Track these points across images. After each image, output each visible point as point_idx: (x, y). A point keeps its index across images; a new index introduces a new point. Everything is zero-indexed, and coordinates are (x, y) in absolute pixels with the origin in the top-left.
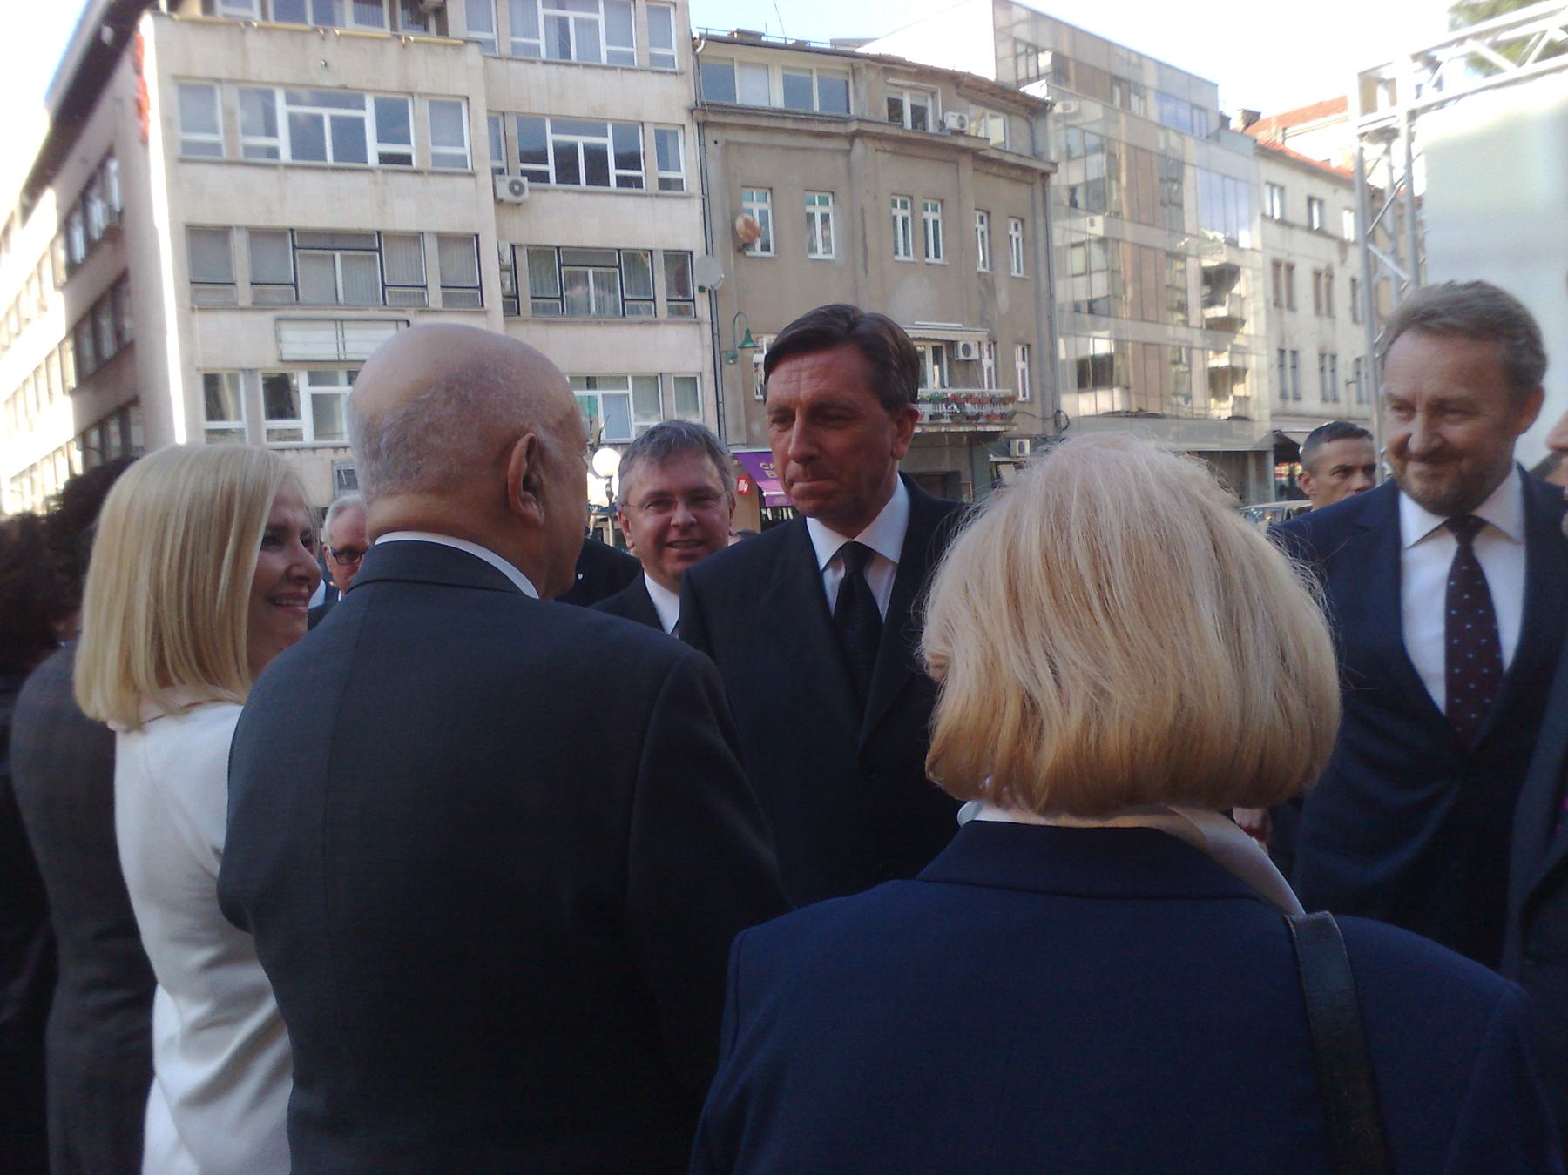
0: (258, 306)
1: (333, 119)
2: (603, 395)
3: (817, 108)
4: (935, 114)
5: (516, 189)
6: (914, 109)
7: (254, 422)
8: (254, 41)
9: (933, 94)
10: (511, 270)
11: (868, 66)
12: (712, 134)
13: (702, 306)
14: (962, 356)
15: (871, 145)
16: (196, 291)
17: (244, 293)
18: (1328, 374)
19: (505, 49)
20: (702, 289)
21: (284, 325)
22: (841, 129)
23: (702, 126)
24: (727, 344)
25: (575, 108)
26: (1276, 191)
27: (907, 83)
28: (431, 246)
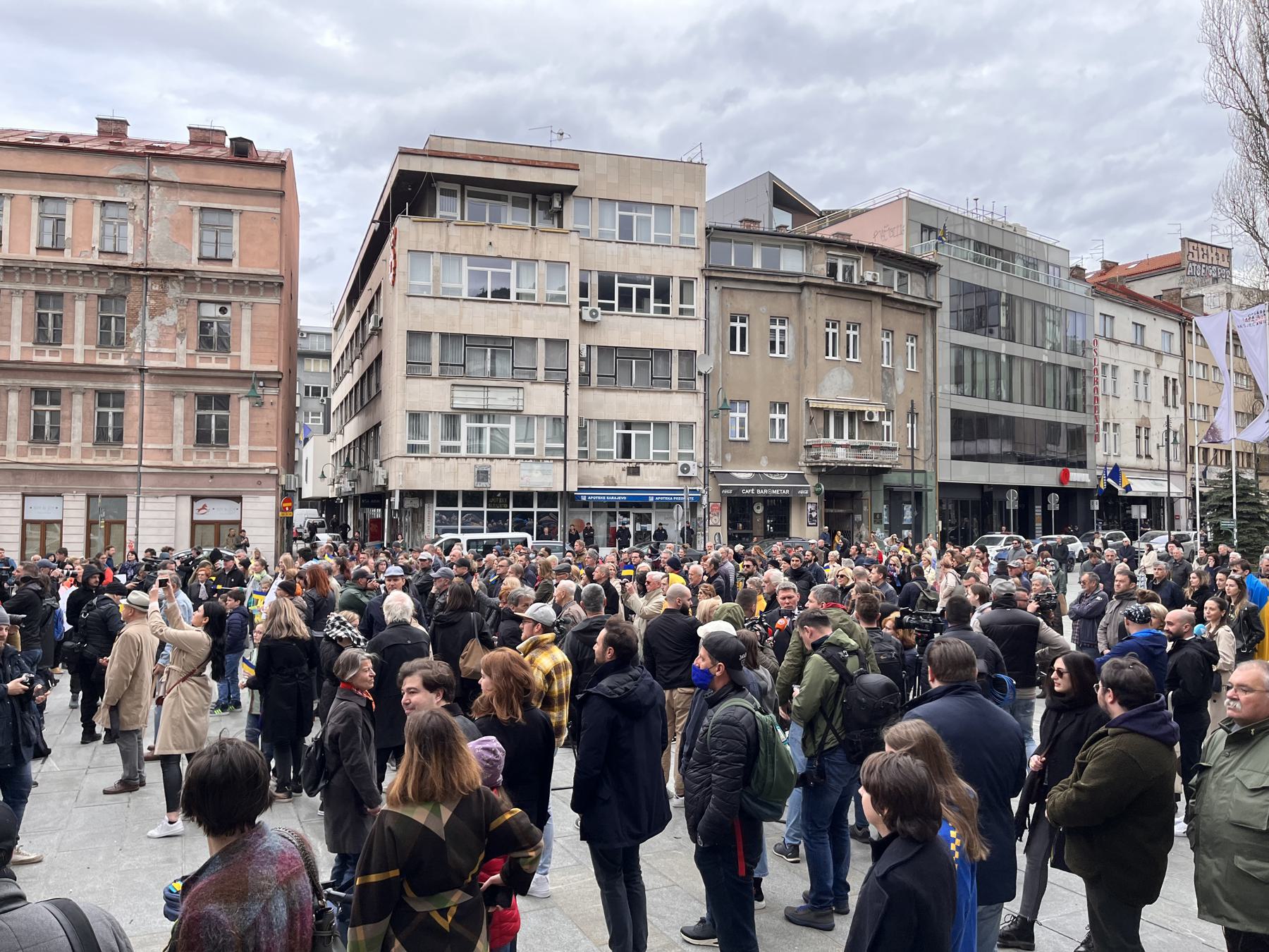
0: (442, 377)
1: (637, 289)
2: (114, 414)
3: (733, 265)
4: (859, 272)
5: (593, 313)
6: (845, 268)
7: (435, 441)
8: (453, 231)
9: (858, 260)
10: (586, 360)
11: (815, 244)
12: (713, 284)
13: (699, 385)
14: (867, 419)
15: (814, 290)
16: (410, 367)
17: (435, 370)
18: (1143, 440)
19: (595, 235)
20: (700, 374)
21: (456, 388)
22: (795, 281)
23: (708, 278)
24: (713, 406)
25: (633, 268)
26: (1139, 327)
27: (841, 254)
28: (541, 345)
